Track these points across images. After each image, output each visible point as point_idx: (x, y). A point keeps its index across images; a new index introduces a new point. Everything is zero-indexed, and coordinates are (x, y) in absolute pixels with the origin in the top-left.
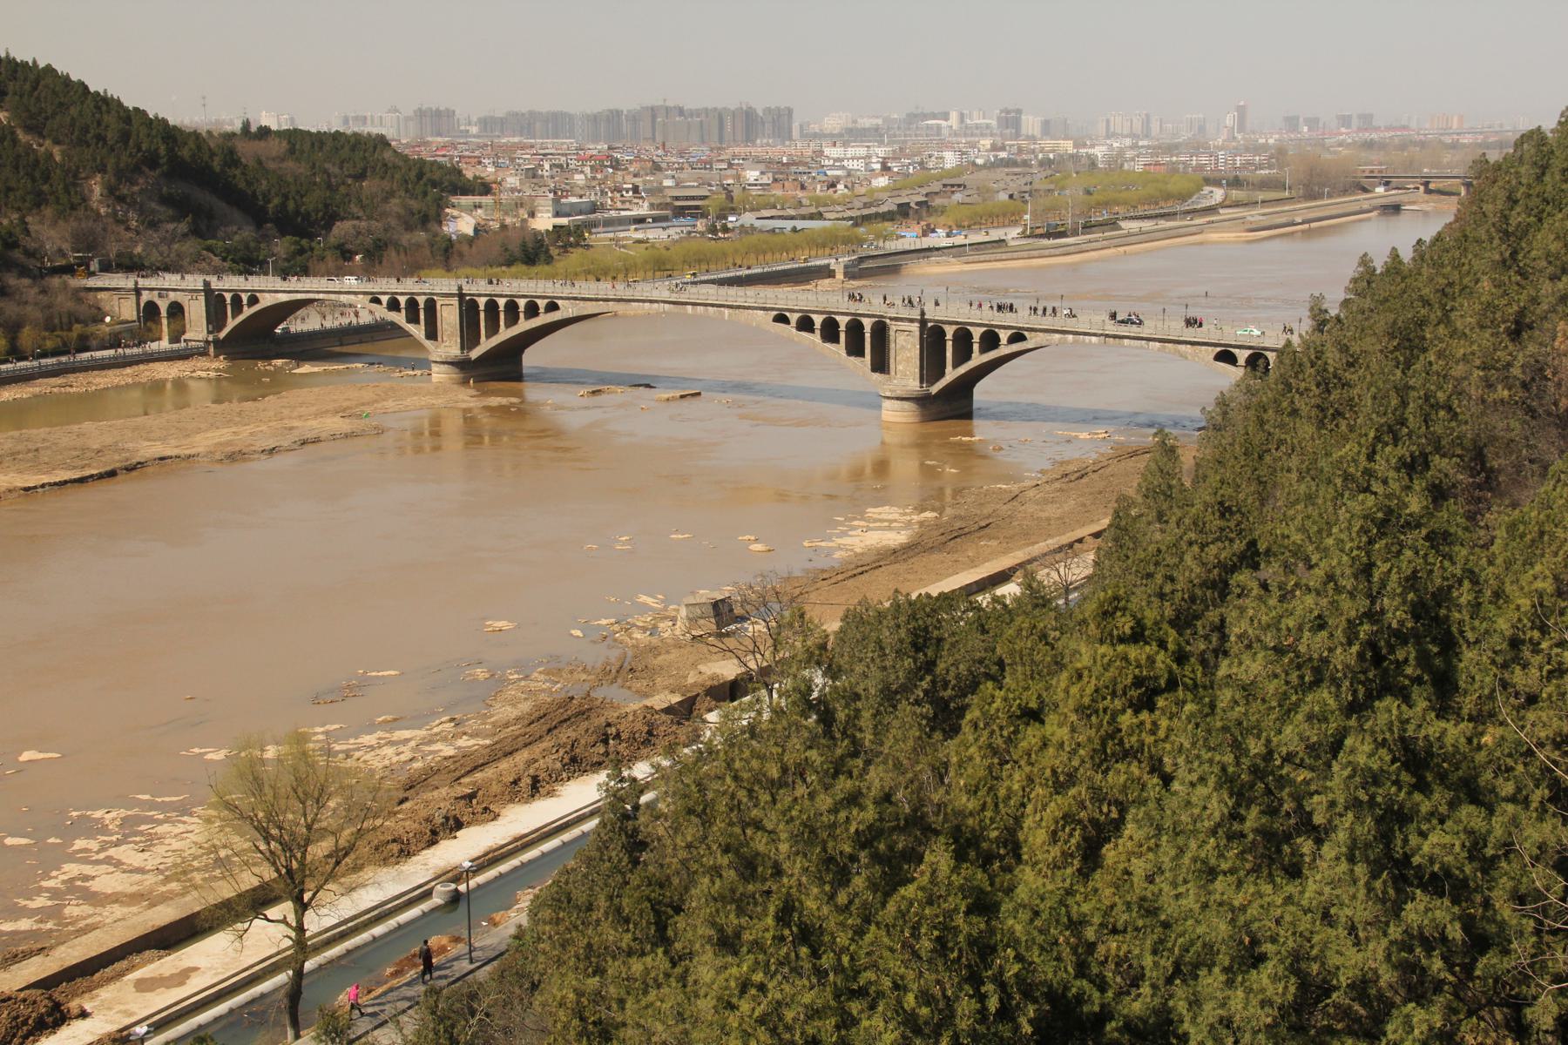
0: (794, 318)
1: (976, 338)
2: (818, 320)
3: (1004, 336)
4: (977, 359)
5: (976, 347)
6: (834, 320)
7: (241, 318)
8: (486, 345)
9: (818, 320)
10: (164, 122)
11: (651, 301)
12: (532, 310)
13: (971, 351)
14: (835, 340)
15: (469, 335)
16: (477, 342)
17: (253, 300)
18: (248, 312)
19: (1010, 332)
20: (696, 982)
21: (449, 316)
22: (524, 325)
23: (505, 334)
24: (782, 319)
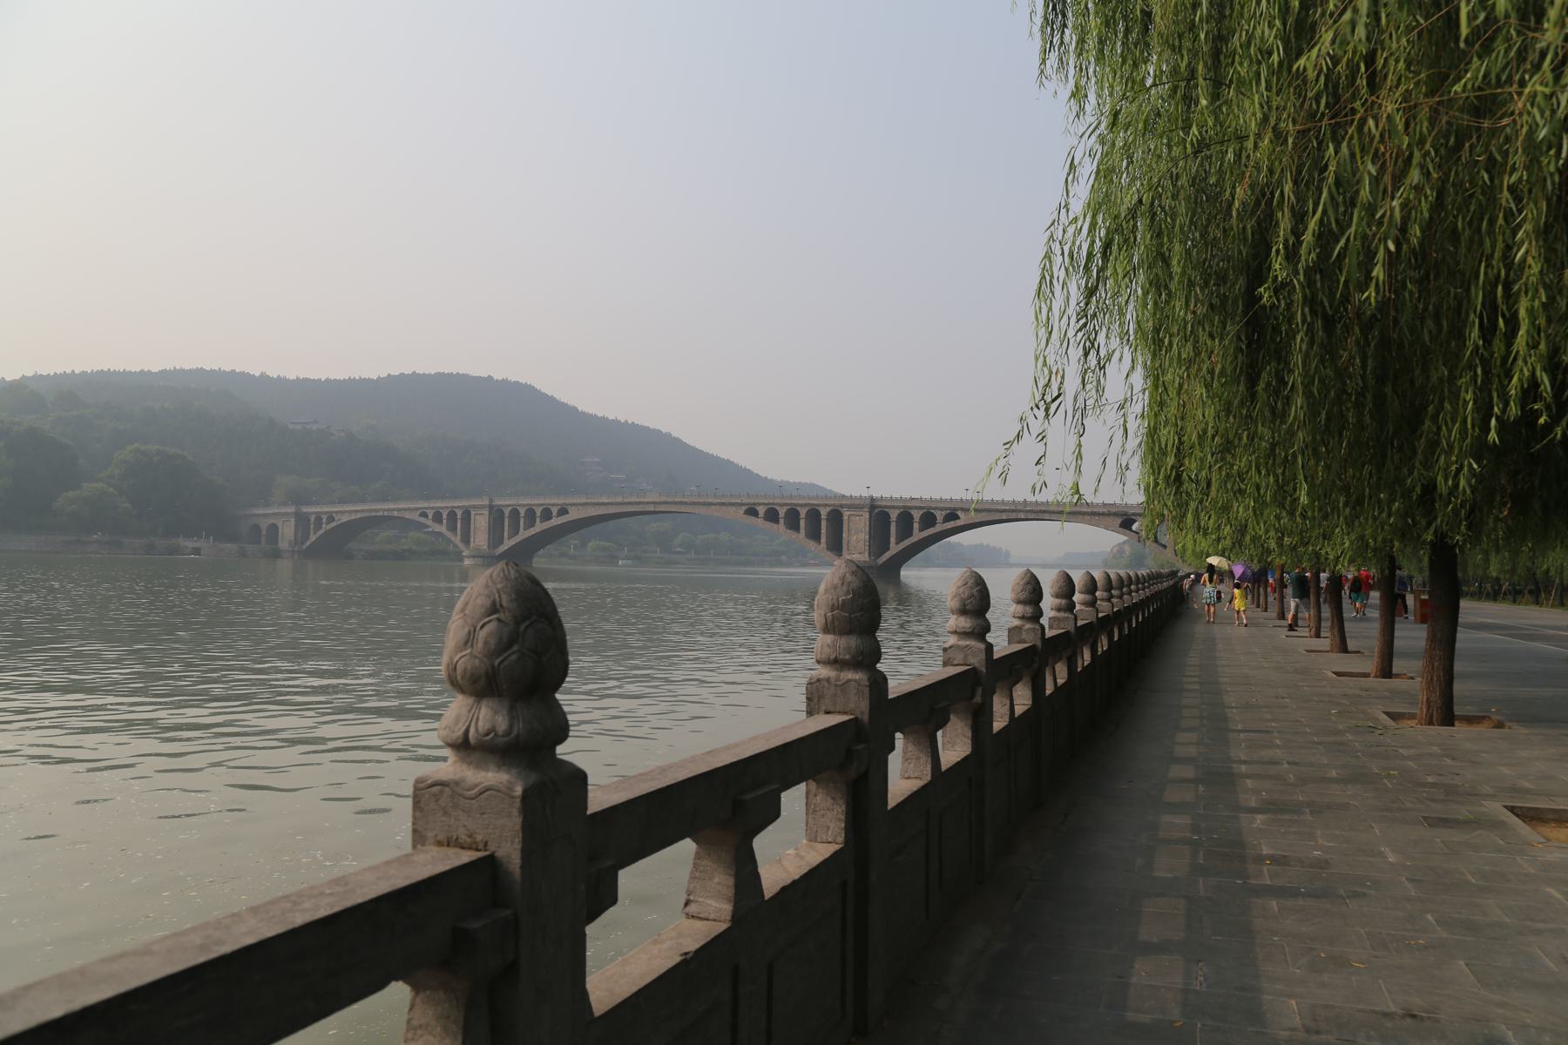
0: (761, 510)
1: (538, 514)
2: (782, 512)
3: (555, 511)
4: (917, 535)
5: (916, 526)
6: (932, 514)
7: (532, 531)
8: (508, 544)
9: (782, 512)
10: (659, 431)
11: (723, 504)
12: (547, 515)
13: (535, 521)
14: (776, 521)
15: (496, 536)
16: (501, 542)
17: (331, 519)
18: (325, 527)
19: (944, 513)
20: (1220, 779)
21: (481, 522)
22: (539, 527)
23: (524, 534)
24: (752, 512)
